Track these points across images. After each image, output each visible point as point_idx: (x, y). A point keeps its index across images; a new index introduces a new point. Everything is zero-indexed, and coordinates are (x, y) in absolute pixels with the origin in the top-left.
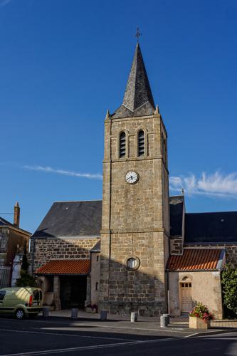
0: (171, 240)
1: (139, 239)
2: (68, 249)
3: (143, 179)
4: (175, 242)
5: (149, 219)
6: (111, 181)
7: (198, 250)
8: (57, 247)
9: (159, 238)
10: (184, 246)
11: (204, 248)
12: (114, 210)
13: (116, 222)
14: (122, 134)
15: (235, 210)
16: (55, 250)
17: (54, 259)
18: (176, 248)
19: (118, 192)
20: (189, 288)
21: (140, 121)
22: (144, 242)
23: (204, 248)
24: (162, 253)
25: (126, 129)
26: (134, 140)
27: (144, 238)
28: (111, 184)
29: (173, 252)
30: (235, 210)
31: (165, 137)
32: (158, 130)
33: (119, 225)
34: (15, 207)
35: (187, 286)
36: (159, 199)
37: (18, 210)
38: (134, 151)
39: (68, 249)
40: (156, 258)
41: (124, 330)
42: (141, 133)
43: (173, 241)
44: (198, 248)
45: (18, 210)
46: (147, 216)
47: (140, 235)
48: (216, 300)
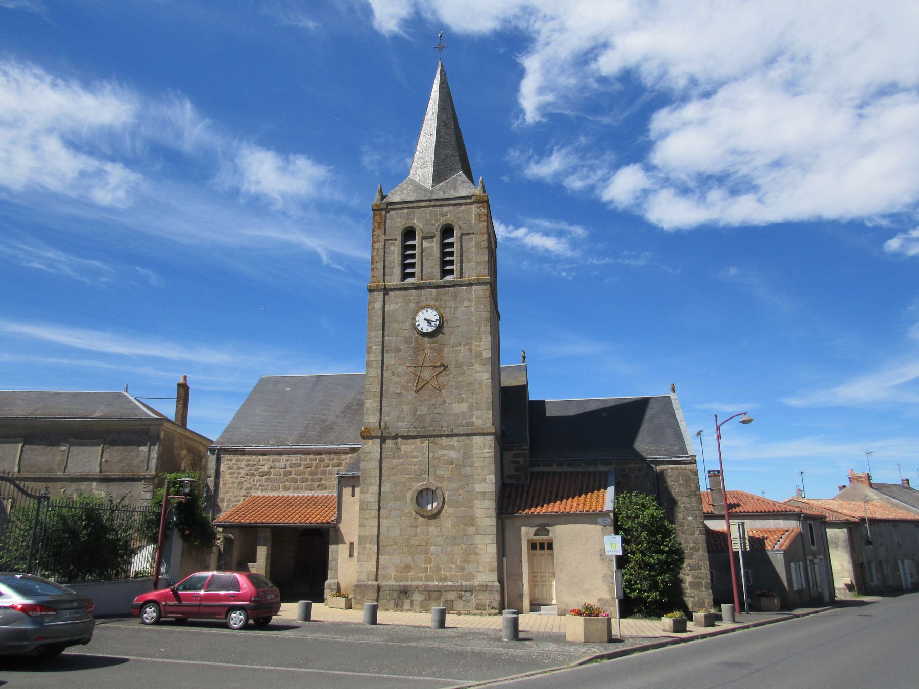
0: (505, 453)
1: (443, 448)
2: (312, 474)
3: (453, 324)
4: (514, 456)
5: (464, 407)
6: (383, 329)
7: (560, 473)
8: (266, 468)
9: (484, 450)
10: (532, 465)
11: (571, 469)
12: (391, 388)
13: (395, 414)
14: (409, 233)
15: (548, 415)
16: (263, 474)
17: (260, 493)
18: (516, 469)
19: (399, 350)
20: (546, 551)
21: (445, 209)
22: (453, 454)
23: (571, 469)
24: (491, 478)
25: (418, 223)
26: (433, 247)
27: (452, 447)
28: (383, 336)
29: (510, 477)
30: (548, 415)
31: (493, 247)
32: (224, 484)
33: (399, 419)
34: (179, 385)
35: (542, 546)
36: (484, 365)
37: (183, 391)
38: (432, 266)
39: (290, 473)
40: (478, 488)
41: (273, 503)
42: (447, 231)
43: (508, 456)
44: (559, 469)
45: (183, 391)
46: (460, 401)
47: (444, 441)
48: (605, 576)
